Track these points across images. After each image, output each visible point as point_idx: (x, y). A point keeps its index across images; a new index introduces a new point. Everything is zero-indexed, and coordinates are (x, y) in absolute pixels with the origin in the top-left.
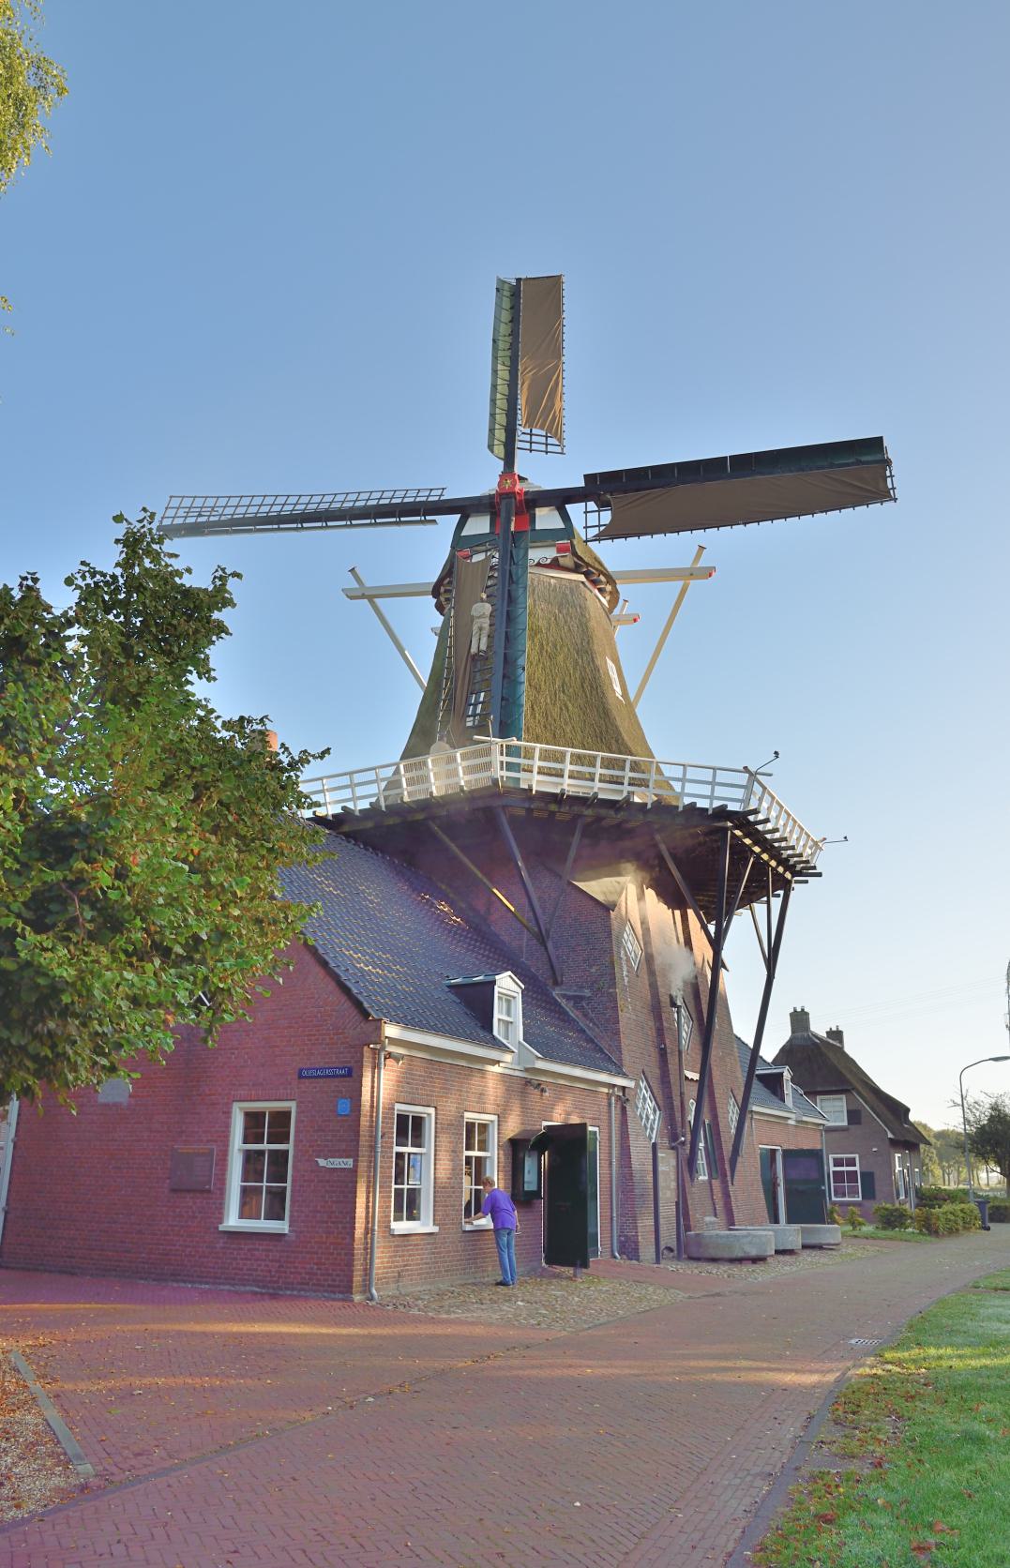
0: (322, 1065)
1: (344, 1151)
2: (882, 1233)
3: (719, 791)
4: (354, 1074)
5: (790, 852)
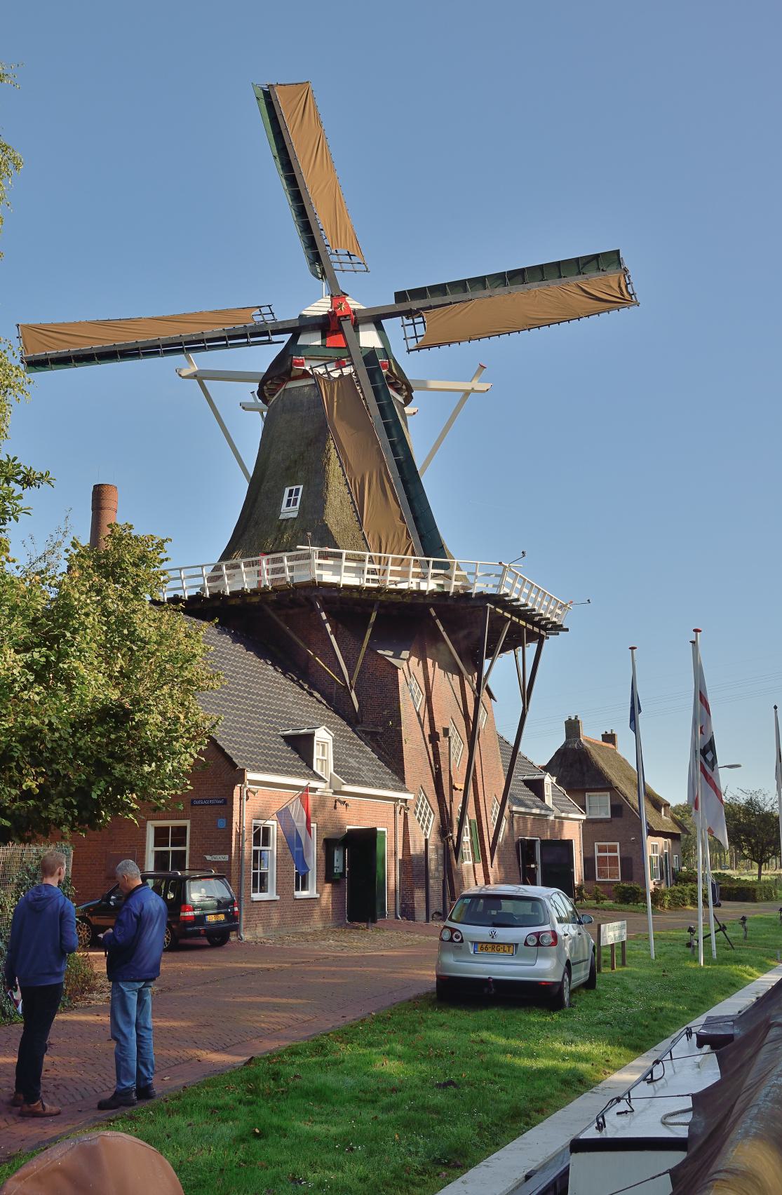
1: (222, 850)
2: (618, 906)
4: (228, 803)
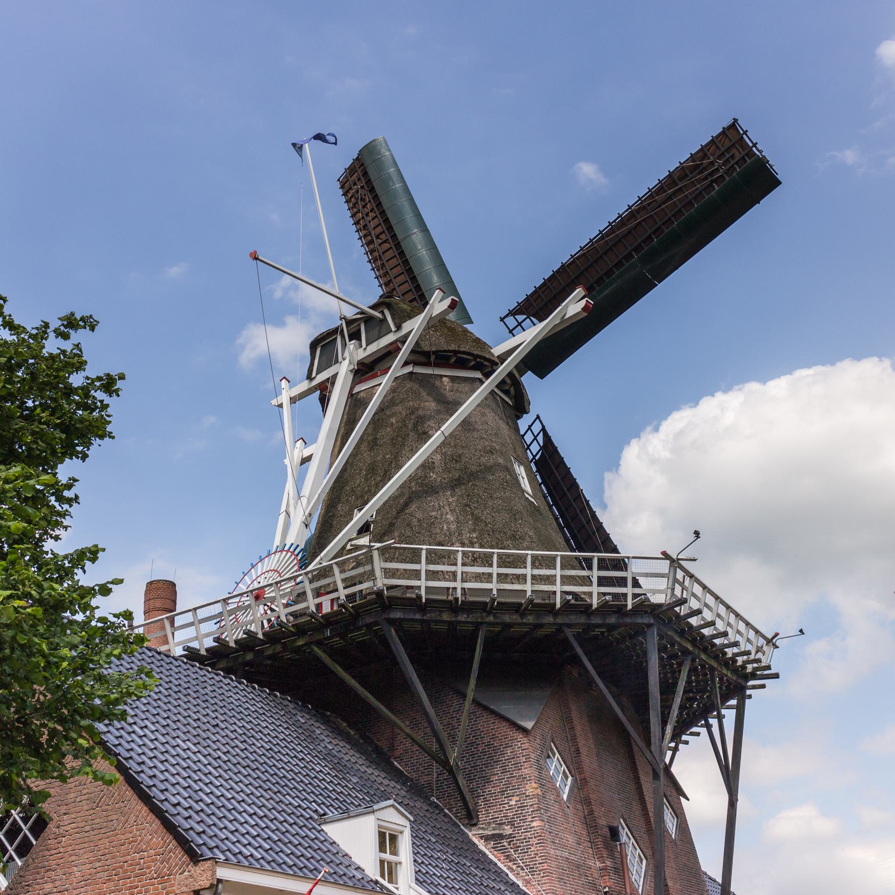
5: (735, 650)
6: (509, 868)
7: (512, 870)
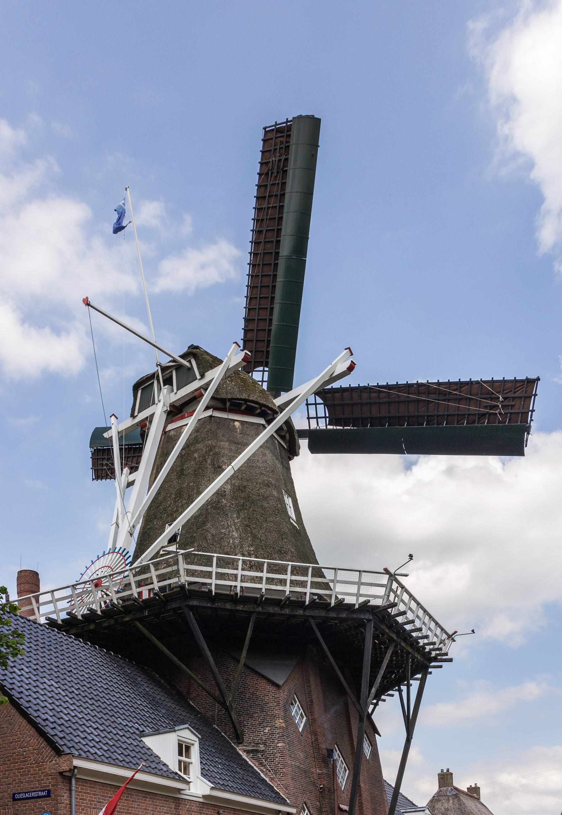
0: (29, 790)
3: (365, 590)
5: (426, 641)
6: (261, 770)
7: (263, 772)
